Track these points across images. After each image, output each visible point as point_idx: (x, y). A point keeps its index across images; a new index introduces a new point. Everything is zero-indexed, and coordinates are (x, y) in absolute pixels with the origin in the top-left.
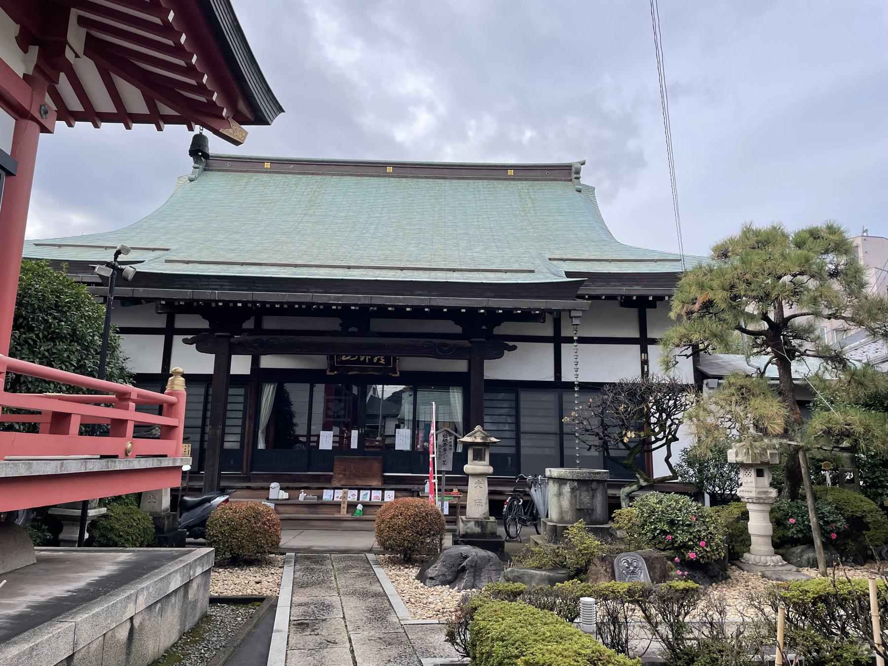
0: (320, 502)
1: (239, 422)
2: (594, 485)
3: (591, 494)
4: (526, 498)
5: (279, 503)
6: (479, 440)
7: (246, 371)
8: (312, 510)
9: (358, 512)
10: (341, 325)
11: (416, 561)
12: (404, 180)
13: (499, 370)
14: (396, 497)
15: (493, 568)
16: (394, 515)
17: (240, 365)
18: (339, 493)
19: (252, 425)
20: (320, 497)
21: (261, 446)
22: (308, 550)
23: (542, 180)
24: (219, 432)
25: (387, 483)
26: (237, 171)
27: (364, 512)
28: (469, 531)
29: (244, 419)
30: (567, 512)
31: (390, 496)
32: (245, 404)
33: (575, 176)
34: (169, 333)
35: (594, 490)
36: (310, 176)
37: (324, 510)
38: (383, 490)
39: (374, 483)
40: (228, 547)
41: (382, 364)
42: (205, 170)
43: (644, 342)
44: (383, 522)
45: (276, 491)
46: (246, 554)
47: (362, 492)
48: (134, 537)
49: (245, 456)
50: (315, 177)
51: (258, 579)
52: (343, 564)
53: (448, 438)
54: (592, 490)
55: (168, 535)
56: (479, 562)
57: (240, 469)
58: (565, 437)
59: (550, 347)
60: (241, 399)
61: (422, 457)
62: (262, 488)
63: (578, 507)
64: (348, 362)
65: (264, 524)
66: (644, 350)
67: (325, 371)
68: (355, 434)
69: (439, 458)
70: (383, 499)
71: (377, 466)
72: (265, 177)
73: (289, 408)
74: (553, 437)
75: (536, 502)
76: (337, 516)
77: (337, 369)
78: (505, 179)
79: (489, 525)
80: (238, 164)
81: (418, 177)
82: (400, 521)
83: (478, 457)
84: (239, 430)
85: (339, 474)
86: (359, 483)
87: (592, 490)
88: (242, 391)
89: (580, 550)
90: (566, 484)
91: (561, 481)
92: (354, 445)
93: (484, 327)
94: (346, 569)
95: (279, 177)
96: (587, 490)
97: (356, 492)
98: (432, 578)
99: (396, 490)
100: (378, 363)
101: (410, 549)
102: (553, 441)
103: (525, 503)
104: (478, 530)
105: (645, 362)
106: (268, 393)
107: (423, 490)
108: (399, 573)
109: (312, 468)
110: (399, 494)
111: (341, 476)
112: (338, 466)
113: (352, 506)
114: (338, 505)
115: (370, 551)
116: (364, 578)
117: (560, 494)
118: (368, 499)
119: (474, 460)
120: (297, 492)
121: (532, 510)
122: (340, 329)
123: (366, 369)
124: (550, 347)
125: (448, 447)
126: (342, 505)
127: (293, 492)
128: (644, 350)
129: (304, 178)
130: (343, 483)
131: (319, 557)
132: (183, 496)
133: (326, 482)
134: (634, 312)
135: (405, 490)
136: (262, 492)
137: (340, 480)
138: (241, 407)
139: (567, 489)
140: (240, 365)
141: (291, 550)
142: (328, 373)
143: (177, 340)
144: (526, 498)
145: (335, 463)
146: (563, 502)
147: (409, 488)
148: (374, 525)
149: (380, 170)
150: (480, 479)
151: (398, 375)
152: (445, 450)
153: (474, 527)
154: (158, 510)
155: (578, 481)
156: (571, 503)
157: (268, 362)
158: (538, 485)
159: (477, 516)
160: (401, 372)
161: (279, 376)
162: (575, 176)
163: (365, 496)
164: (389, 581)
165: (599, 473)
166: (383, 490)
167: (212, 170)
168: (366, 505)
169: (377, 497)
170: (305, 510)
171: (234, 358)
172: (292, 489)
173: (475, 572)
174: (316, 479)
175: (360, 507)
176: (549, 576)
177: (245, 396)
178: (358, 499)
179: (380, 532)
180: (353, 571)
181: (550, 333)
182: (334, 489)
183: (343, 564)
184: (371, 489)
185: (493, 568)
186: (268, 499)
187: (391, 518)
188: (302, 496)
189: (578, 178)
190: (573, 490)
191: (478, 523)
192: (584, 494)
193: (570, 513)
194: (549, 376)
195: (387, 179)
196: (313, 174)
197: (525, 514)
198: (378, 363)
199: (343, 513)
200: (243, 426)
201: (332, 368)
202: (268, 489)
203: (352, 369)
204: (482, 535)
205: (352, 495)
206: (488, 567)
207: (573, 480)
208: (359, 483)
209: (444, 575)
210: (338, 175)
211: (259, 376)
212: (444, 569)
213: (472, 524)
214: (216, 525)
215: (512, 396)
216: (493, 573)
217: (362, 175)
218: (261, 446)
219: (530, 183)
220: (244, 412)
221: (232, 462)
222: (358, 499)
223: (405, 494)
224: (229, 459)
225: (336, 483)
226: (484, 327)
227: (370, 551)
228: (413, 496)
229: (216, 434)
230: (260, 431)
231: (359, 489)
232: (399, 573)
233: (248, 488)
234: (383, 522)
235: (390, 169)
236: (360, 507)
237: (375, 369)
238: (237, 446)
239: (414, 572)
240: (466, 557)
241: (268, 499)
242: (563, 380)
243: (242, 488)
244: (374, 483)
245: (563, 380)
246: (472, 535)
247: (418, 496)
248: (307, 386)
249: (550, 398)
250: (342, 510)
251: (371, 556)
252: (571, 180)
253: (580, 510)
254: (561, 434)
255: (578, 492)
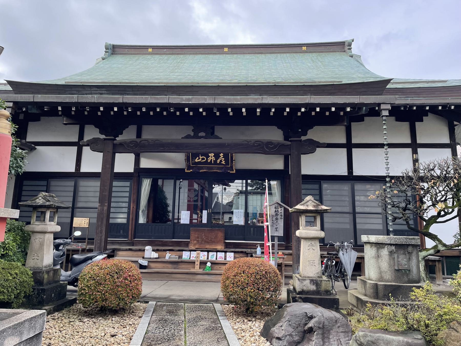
0: (180, 260)
1: (126, 205)
2: (410, 249)
3: (408, 257)
4: (337, 260)
5: (151, 261)
6: (311, 208)
7: (130, 169)
8: (175, 266)
9: (207, 268)
10: (193, 131)
11: (257, 313)
12: (235, 55)
13: (311, 165)
14: (235, 258)
15: (341, 329)
16: (237, 273)
17: (124, 163)
18: (194, 254)
19: (135, 207)
20: (180, 257)
21: (142, 220)
22: (167, 299)
23: (325, 52)
24: (105, 208)
25: (228, 247)
26: (132, 54)
27: (212, 268)
28: (305, 288)
29: (129, 203)
30: (386, 272)
31: (230, 256)
32: (130, 192)
33: (349, 47)
34: (79, 146)
35: (410, 253)
36: (176, 55)
37: (183, 266)
38: (225, 252)
39: (219, 247)
40: (93, 299)
41: (223, 164)
42: (112, 54)
43: (414, 146)
44: (228, 278)
45: (150, 252)
46: (113, 302)
47: (211, 254)
48: (10, 290)
49: (130, 228)
50: (179, 55)
51: (113, 331)
52: (194, 315)
53: (280, 209)
54: (409, 253)
55: (45, 287)
56: (326, 323)
57: (126, 237)
58: (357, 215)
59: (344, 151)
60: (128, 189)
61: (252, 229)
62: (140, 250)
63: (396, 268)
64: (199, 163)
65: (126, 279)
66: (415, 152)
67: (184, 169)
68: (205, 213)
69: (272, 226)
70: (225, 259)
71: (221, 235)
72: (149, 57)
73: (165, 201)
74: (347, 215)
75: (344, 262)
76: (192, 270)
77: (192, 168)
78: (301, 52)
79: (323, 284)
80: (133, 50)
81: (244, 53)
82: (243, 278)
83: (310, 223)
84: (126, 210)
85: (194, 240)
86: (208, 247)
87: (409, 253)
88: (128, 184)
89: (441, 316)
90: (384, 248)
91: (379, 245)
92: (205, 221)
93: (300, 130)
94: (196, 320)
95: (157, 57)
96: (404, 254)
97: (206, 253)
98: (279, 339)
99: (235, 252)
100: (220, 163)
101: (252, 304)
102: (348, 219)
103: (337, 263)
104: (313, 288)
105: (415, 161)
106: (146, 184)
107: (256, 253)
108: (244, 327)
109: (178, 237)
110: (237, 255)
111: (195, 242)
112: (193, 235)
113: (203, 264)
114: (194, 263)
115: (217, 301)
116: (212, 333)
117: (378, 257)
118: (214, 259)
119: (306, 225)
120: (164, 253)
121: (341, 269)
122: (192, 134)
123: (212, 168)
124: (344, 151)
125: (279, 217)
126: (196, 263)
127: (161, 253)
128: (415, 152)
129: (173, 57)
130: (197, 247)
131: (175, 306)
132: (73, 255)
133: (184, 246)
134: (406, 125)
135: (242, 252)
136: (140, 253)
137: (195, 245)
138: (127, 194)
139: (385, 252)
140: (124, 163)
141: (154, 299)
142: (186, 171)
143: (86, 150)
144: (337, 260)
145: (191, 233)
146: (382, 264)
147: (243, 251)
148: (220, 278)
149: (220, 50)
150: (313, 242)
151: (234, 172)
152: (277, 219)
153: (309, 285)
154: (41, 266)
155: (396, 245)
156: (390, 266)
157: (145, 163)
158: (344, 250)
159: (311, 275)
160: (236, 170)
161: (156, 174)
162: (349, 47)
163: (213, 256)
164: (236, 337)
165: (414, 239)
166: (225, 252)
167: (117, 54)
168: (213, 263)
169: (221, 257)
170: (170, 266)
171: (118, 156)
172: (161, 250)
173: (323, 334)
174: (178, 244)
175: (209, 264)
176: (407, 343)
177: (130, 187)
178: (208, 258)
179: (225, 288)
180: (203, 323)
181: (343, 140)
182: (191, 251)
183: (194, 315)
184: (217, 251)
185: (341, 329)
186: (143, 258)
187: (235, 276)
188: (168, 256)
189: (350, 49)
190: (391, 253)
191: (313, 281)
192: (401, 257)
193: (389, 273)
194: (344, 172)
195: (224, 55)
196: (178, 54)
197: (337, 271)
198: (220, 163)
199: (197, 269)
200: (129, 208)
201: (189, 167)
202: (144, 250)
203: (202, 168)
204: (317, 292)
205: (203, 256)
206: (335, 329)
207: (391, 245)
208: (208, 247)
209: (291, 335)
210: (193, 54)
211: (140, 173)
212: (291, 330)
213: (307, 282)
214: (84, 279)
215: (317, 186)
216: (342, 335)
217: (208, 54)
218: (364, 108)
219: (318, 54)
220: (130, 197)
221: (121, 232)
222: (208, 258)
223: (241, 255)
224: (114, 230)
225: (192, 247)
226: (300, 130)
227: (217, 301)
228: (247, 257)
229: (103, 210)
230: (140, 211)
231: (208, 251)
232: (244, 327)
233: (130, 250)
234: (228, 278)
235: (226, 50)
236: (209, 264)
237: (218, 168)
238: (124, 221)
239: (257, 325)
240: (311, 318)
241: (143, 258)
242: (354, 174)
243: (126, 250)
244: (219, 247)
245: (354, 174)
246: (308, 292)
247: (252, 256)
248: (173, 181)
249: (346, 187)
250: (196, 266)
251: (218, 306)
252: (345, 51)
253: (398, 270)
254: (354, 213)
255: (396, 256)
